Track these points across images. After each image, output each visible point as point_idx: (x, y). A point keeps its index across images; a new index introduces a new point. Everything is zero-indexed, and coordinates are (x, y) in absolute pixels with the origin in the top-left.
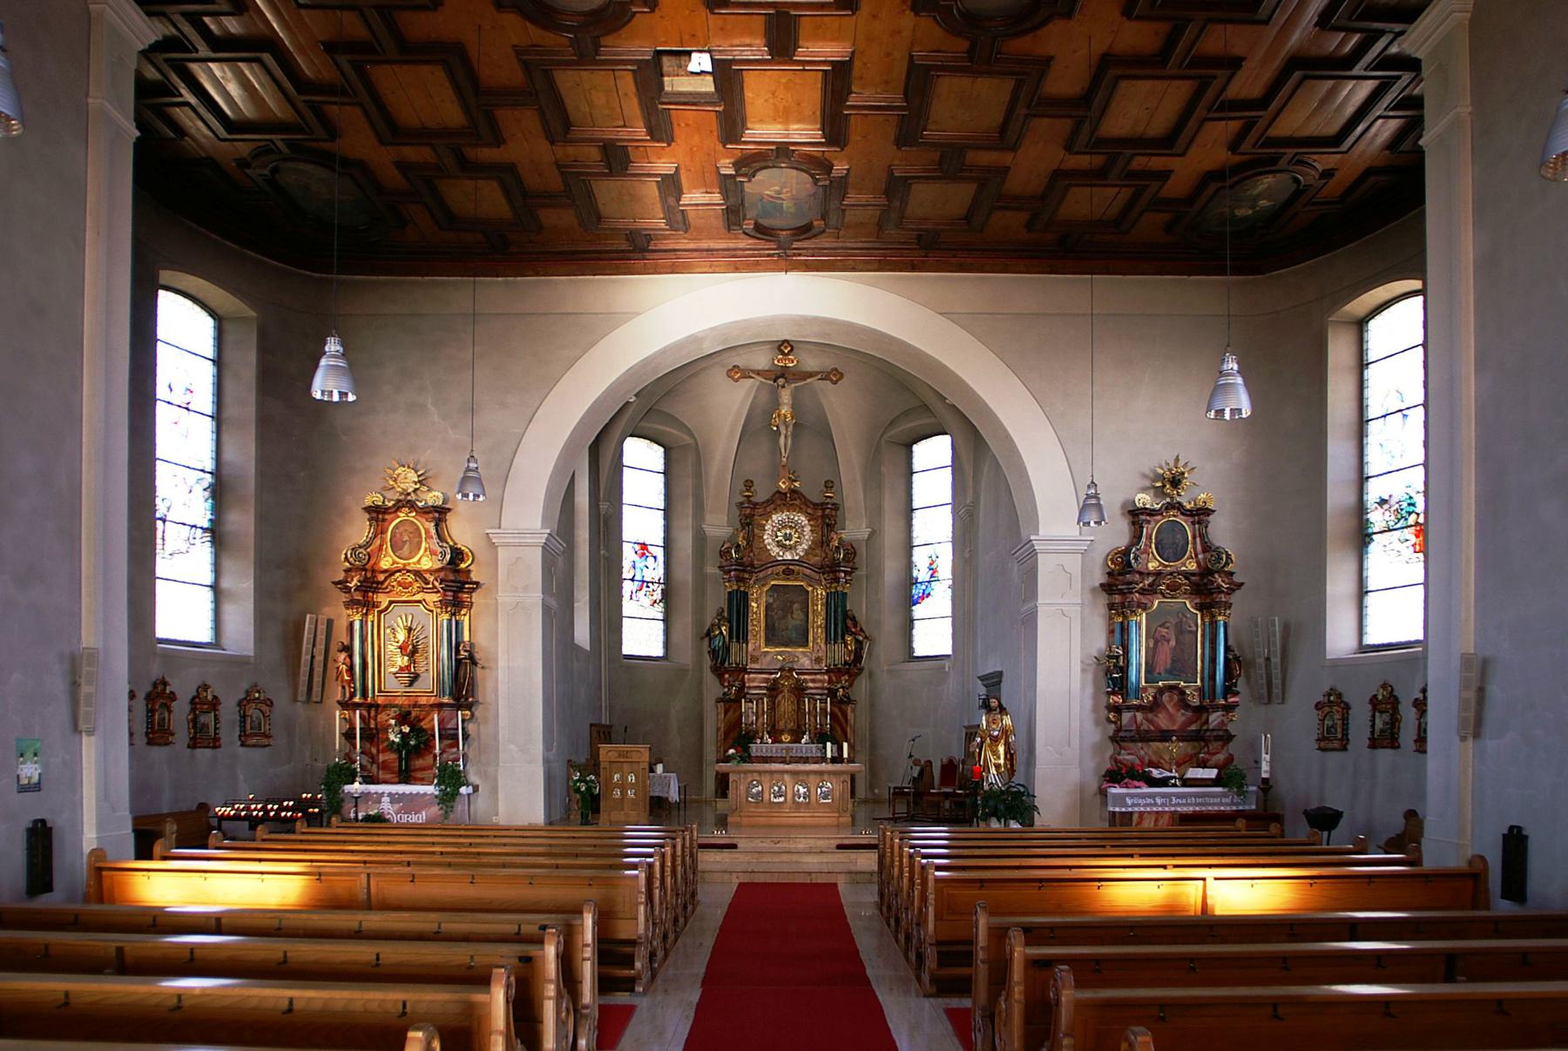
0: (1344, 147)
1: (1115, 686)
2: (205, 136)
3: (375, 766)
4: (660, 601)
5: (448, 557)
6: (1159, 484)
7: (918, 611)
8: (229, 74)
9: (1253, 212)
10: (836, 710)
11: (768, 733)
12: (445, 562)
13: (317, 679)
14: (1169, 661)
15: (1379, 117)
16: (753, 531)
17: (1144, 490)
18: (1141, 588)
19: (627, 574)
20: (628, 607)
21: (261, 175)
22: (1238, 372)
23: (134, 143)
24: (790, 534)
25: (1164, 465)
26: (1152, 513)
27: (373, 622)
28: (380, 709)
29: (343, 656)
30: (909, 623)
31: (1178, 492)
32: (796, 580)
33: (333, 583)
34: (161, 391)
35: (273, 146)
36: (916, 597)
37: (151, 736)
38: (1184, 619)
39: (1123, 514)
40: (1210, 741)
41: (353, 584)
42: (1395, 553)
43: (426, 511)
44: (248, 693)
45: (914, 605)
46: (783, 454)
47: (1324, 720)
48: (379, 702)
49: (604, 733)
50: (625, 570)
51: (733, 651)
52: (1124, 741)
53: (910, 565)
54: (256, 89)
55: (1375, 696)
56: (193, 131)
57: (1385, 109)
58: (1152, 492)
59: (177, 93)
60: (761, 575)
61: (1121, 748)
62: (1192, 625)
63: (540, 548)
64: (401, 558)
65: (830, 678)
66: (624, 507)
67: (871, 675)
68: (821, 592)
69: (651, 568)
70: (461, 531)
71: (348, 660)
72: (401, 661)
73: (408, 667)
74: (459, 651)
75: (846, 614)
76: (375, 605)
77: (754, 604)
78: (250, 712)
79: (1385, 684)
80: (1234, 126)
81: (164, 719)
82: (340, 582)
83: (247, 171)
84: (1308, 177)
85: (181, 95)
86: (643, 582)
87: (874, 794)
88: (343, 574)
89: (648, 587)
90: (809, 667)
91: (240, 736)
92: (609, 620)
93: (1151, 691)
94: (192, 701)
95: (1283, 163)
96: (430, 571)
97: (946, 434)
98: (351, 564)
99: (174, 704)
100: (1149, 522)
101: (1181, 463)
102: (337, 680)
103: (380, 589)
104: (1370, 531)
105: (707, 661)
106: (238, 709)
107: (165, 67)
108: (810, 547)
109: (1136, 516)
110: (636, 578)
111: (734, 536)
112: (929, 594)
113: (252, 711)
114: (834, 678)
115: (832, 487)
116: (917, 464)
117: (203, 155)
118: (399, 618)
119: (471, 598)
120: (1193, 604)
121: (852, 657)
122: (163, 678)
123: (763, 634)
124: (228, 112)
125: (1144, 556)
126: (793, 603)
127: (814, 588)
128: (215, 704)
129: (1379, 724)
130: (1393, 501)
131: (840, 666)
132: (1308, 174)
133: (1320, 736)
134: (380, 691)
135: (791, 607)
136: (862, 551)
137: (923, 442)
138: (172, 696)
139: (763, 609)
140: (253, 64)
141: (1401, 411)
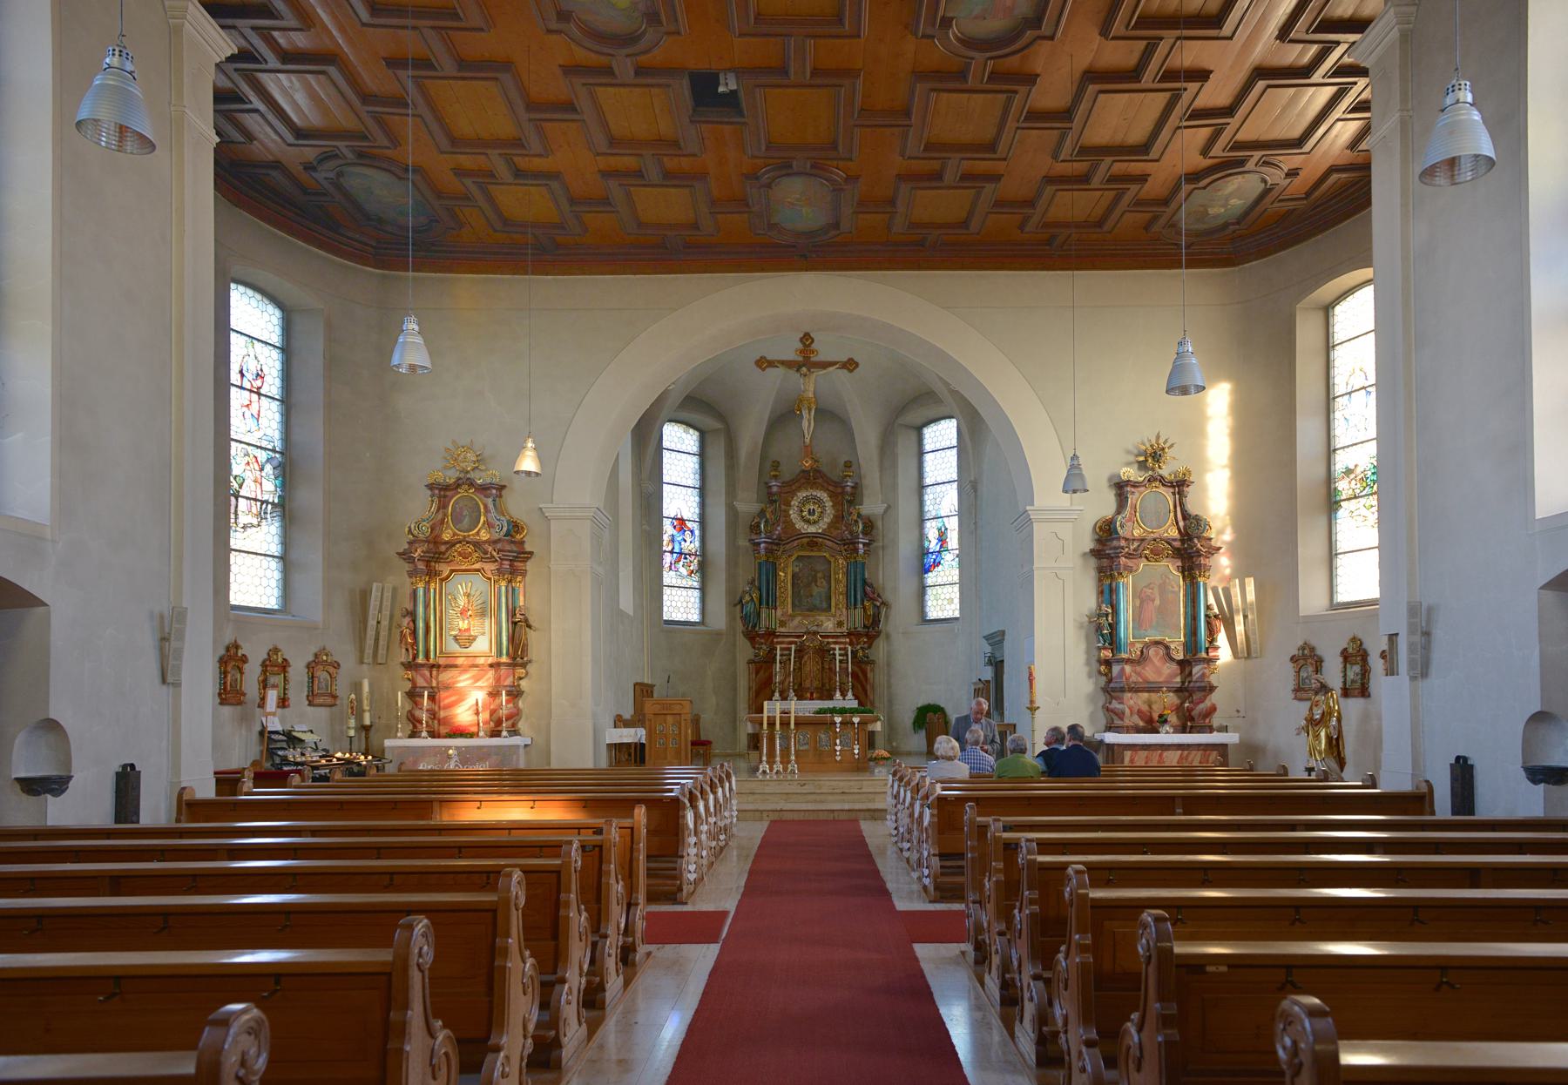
0: (1307, 148)
1: (1105, 641)
2: (273, 140)
3: (436, 722)
4: (697, 571)
5: (505, 529)
6: (1142, 459)
8: (297, 84)
9: (1225, 211)
10: (856, 669)
12: (502, 533)
13: (382, 642)
15: (1338, 120)
16: (780, 506)
17: (1128, 464)
18: (1127, 553)
20: (669, 577)
21: (326, 178)
23: (215, 148)
24: (813, 510)
25: (1146, 441)
26: (1136, 485)
27: (435, 589)
28: (441, 669)
29: (406, 621)
30: (922, 590)
31: (1159, 466)
32: (819, 550)
33: (397, 553)
34: (235, 378)
35: (338, 152)
37: (224, 696)
38: (1167, 581)
40: (1194, 692)
41: (417, 554)
42: (1362, 519)
43: (484, 489)
44: (316, 655)
45: (926, 573)
46: (807, 436)
47: (1299, 672)
48: (441, 663)
49: (647, 691)
50: (665, 543)
51: (763, 615)
53: (922, 536)
54: (323, 99)
55: (1345, 649)
56: (261, 136)
57: (1344, 112)
58: (1136, 466)
59: (247, 101)
64: (461, 531)
65: (851, 640)
67: (888, 636)
69: (688, 540)
70: (517, 506)
71: (411, 624)
74: (515, 615)
75: (865, 582)
76: (437, 573)
77: (781, 573)
78: (318, 674)
79: (1354, 638)
80: (1205, 133)
81: (236, 680)
82: (403, 554)
83: (313, 174)
84: (1275, 176)
85: (251, 103)
86: (681, 553)
87: (892, 747)
88: (406, 546)
90: (832, 631)
91: (308, 696)
92: (652, 591)
93: (1139, 646)
94: (264, 665)
95: (1250, 165)
96: (488, 542)
97: (953, 417)
98: (414, 536)
99: (246, 666)
101: (1161, 441)
102: (401, 642)
103: (442, 558)
104: (1338, 498)
105: (740, 626)
106: (307, 670)
107: (236, 76)
108: (832, 522)
109: (1121, 488)
111: (762, 513)
113: (322, 675)
114: (854, 640)
115: (850, 467)
117: (271, 158)
118: (459, 586)
119: (525, 566)
120: (1175, 566)
121: (871, 621)
122: (236, 641)
123: (790, 600)
124: (295, 118)
125: (1130, 524)
126: (817, 572)
127: (836, 559)
128: (284, 666)
129: (1351, 675)
130: (1359, 470)
131: (859, 629)
132: (1274, 174)
133: (1296, 687)
134: (441, 652)
136: (879, 524)
138: (244, 659)
139: (790, 577)
140: (320, 76)
141: (1364, 388)
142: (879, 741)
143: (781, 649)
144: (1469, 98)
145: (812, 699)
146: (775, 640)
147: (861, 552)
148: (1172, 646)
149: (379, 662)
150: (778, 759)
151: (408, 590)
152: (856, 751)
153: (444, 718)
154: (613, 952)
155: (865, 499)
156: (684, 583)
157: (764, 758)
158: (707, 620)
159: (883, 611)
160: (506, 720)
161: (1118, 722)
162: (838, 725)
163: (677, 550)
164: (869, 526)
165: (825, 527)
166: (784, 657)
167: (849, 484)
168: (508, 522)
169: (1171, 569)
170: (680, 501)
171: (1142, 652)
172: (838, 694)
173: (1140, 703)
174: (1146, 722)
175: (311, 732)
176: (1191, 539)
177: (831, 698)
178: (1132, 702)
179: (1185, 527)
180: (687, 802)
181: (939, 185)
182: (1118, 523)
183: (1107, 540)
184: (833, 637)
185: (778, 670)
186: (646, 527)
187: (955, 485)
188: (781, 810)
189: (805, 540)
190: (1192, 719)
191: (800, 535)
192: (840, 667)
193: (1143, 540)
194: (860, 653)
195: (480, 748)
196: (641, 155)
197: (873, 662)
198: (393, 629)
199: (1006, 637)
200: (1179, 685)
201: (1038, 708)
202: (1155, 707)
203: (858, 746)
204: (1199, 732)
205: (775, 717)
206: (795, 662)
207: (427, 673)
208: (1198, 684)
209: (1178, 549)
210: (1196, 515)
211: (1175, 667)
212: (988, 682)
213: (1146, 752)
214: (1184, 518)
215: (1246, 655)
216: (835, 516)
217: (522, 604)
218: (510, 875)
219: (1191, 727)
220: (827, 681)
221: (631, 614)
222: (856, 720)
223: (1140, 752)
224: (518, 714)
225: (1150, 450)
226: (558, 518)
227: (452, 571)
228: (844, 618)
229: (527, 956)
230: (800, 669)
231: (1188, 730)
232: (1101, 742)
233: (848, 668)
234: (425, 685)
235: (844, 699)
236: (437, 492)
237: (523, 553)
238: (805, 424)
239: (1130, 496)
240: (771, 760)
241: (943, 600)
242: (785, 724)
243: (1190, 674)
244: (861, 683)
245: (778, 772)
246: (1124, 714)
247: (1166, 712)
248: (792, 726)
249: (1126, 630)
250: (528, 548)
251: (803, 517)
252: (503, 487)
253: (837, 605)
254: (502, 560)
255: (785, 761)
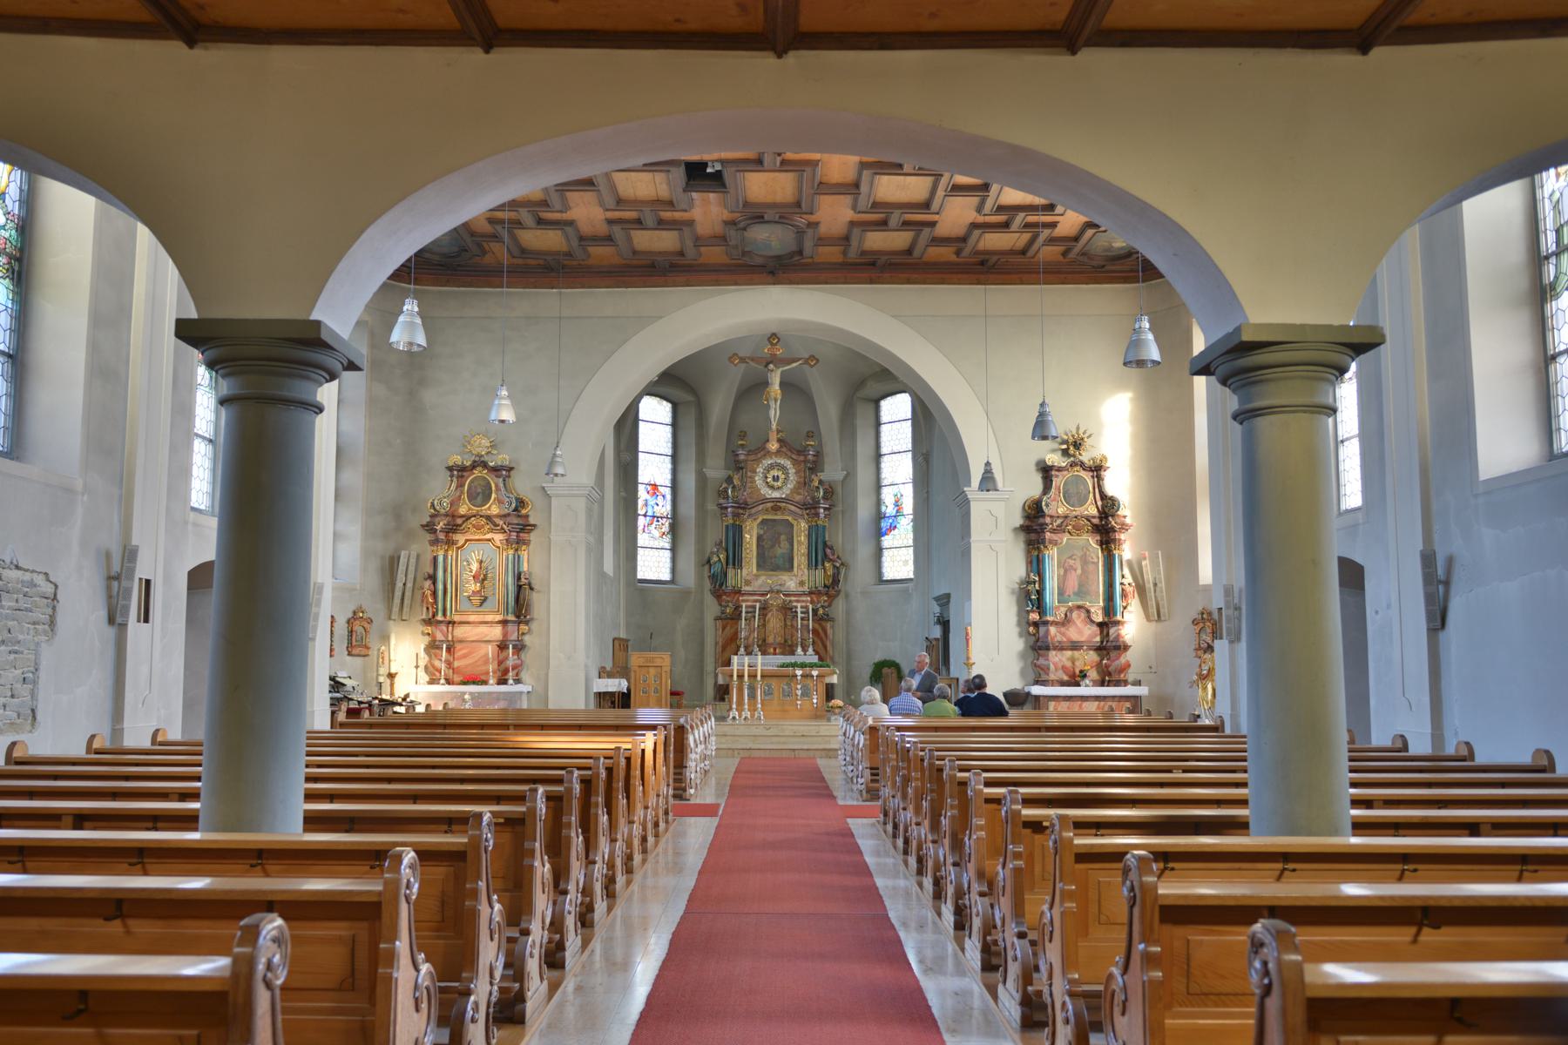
1: (1033, 606)
3: (451, 671)
5: (514, 505)
6: (1064, 447)
7: (887, 541)
10: (817, 626)
11: (758, 646)
14: (1076, 584)
16: (746, 473)
17: (1054, 451)
19: (641, 512)
20: (642, 539)
22: (1149, 329)
24: (778, 476)
26: (1060, 469)
28: (456, 625)
30: (879, 552)
32: (783, 514)
36: (884, 530)
39: (1038, 470)
43: (496, 470)
44: (355, 613)
45: (883, 536)
52: (1040, 649)
53: (879, 502)
58: (1060, 453)
60: (753, 511)
61: (1039, 655)
62: (1094, 557)
63: (583, 500)
65: (812, 598)
66: (640, 454)
67: (847, 596)
68: (803, 525)
69: (661, 504)
70: (522, 484)
71: (432, 587)
72: (473, 587)
73: (479, 592)
75: (825, 544)
78: (355, 628)
82: (427, 526)
86: (654, 517)
89: (658, 521)
91: (347, 647)
92: (629, 551)
93: (1063, 610)
96: (497, 516)
100: (1057, 476)
101: (1081, 432)
105: (708, 585)
106: (347, 625)
108: (795, 487)
110: (648, 514)
111: (729, 480)
112: (895, 527)
113: (358, 628)
114: (815, 599)
116: (885, 417)
121: (831, 581)
126: (780, 534)
131: (820, 588)
133: (1197, 646)
134: (456, 611)
135: (779, 537)
136: (839, 490)
137: (889, 398)
142: (838, 691)
143: (746, 607)
144: (1147, 326)
145: (775, 654)
146: (741, 598)
147: (822, 516)
148: (1092, 610)
149: (404, 618)
150: (746, 707)
151: (428, 557)
152: (815, 701)
153: (458, 667)
154: (536, 952)
155: (826, 466)
156: (656, 544)
157: (734, 706)
158: (679, 578)
159: (843, 571)
160: (513, 669)
161: (1044, 677)
162: (799, 678)
163: (650, 513)
164: (830, 493)
165: (788, 492)
166: (749, 615)
167: (811, 453)
168: (517, 499)
169: (1092, 541)
170: (654, 467)
171: (1066, 615)
172: (799, 650)
173: (1064, 659)
174: (1070, 677)
175: (350, 678)
176: (1107, 517)
177: (793, 653)
178: (1057, 659)
179: (1102, 505)
180: (689, 728)
181: (899, 172)
182: (1043, 503)
183: (1035, 517)
184: (795, 595)
185: (743, 626)
186: (623, 494)
187: (910, 454)
188: (750, 749)
189: (769, 505)
190: (1110, 674)
191: (765, 500)
192: (801, 623)
193: (1066, 517)
194: (821, 611)
195: (490, 693)
196: (642, 211)
197: (832, 620)
198: (416, 591)
199: (951, 600)
200: (1098, 644)
201: (974, 663)
202: (1077, 663)
203: (816, 697)
204: (1115, 686)
205: (743, 670)
206: (759, 619)
207: (445, 628)
208: (1114, 644)
209: (1096, 525)
210: (1112, 497)
211: (1096, 629)
212: (937, 639)
213: (1068, 703)
214: (1102, 499)
215: (1156, 618)
216: (798, 483)
217: (525, 569)
218: (398, 858)
219: (1109, 681)
220: (790, 637)
221: (611, 575)
222: (815, 673)
223: (1063, 703)
224: (521, 665)
225: (1071, 440)
226: (558, 496)
227: (467, 541)
228: (805, 578)
229: (421, 961)
230: (764, 625)
231: (1106, 684)
232: (1028, 694)
233: (808, 626)
234: (443, 638)
235: (805, 654)
236: (455, 473)
237: (530, 525)
238: (772, 413)
239: (1054, 479)
240: (740, 708)
241: (899, 562)
242: (753, 676)
243: (1108, 634)
244: (821, 642)
245: (745, 719)
246: (1049, 669)
247: (1086, 668)
248: (759, 678)
249: (1051, 597)
250: (532, 521)
251: (767, 483)
252: (512, 469)
253: (799, 565)
254: (510, 531)
255: (753, 709)
